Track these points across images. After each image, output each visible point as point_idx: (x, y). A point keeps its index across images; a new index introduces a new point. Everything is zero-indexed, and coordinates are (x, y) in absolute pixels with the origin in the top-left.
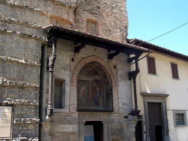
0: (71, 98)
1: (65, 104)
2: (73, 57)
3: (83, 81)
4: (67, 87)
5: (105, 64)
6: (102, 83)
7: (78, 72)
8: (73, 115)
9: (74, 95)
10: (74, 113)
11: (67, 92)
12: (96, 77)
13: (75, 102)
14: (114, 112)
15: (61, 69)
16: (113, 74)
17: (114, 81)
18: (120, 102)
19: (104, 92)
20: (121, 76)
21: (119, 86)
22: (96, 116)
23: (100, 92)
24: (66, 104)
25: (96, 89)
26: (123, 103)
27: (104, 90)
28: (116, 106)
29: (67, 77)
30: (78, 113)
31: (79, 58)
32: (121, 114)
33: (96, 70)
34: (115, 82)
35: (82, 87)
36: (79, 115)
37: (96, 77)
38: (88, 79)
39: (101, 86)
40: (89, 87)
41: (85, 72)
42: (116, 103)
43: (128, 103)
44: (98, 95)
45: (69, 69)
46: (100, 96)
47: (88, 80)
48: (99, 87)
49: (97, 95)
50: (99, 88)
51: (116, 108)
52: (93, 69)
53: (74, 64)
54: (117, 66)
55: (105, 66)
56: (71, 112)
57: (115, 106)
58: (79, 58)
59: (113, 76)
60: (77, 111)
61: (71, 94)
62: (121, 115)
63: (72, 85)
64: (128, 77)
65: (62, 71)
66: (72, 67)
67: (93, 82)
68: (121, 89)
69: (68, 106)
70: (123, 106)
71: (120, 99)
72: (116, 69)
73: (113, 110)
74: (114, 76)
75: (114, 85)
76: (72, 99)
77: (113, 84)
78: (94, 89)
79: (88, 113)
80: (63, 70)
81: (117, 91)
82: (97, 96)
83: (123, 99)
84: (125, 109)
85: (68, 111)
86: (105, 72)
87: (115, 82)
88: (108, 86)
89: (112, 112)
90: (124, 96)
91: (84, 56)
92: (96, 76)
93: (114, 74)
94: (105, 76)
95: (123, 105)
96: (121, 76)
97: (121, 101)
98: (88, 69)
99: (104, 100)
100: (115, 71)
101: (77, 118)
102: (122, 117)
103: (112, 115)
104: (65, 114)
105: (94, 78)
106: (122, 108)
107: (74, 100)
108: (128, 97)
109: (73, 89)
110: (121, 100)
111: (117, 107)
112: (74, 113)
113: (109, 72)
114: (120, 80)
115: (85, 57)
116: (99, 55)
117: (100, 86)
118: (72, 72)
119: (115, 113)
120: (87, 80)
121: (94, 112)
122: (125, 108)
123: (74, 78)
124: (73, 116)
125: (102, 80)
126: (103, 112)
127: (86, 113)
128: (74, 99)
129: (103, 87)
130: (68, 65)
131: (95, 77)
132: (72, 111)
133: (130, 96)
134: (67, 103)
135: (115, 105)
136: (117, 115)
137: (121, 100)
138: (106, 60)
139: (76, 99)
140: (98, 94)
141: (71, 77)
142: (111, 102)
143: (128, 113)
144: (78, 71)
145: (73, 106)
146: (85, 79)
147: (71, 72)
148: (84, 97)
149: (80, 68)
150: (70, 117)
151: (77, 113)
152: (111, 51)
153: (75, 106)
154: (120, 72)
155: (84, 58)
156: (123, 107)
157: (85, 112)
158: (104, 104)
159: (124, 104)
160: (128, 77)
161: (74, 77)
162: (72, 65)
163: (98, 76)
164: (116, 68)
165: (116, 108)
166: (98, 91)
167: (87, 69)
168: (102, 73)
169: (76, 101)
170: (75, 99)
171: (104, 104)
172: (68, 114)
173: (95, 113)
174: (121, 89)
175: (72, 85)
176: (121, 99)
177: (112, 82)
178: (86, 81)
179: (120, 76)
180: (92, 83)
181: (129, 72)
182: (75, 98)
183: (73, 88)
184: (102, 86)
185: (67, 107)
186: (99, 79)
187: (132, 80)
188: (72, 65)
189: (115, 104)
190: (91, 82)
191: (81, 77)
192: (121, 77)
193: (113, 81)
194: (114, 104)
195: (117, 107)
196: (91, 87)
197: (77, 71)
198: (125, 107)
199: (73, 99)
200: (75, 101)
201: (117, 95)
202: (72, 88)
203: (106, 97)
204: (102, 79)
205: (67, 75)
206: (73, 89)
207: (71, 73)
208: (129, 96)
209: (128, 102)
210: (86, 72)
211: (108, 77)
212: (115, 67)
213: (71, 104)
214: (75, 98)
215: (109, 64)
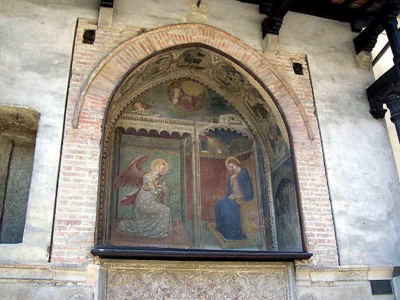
0: (64, 191)
1: (27, 222)
2: (92, 27)
3: (158, 136)
4: (48, 141)
5: (248, 54)
6: (255, 144)
7: (112, 82)
8: (72, 276)
9: (79, 181)
10: (74, 267)
11: (42, 166)
12: (224, 119)
13: (86, 211)
14: (314, 261)
15: (26, 68)
16: (289, 91)
17: (301, 120)
18: (341, 213)
19: (263, 181)
20: (333, 100)
21: (330, 143)
22: (211, 286)
23: (245, 180)
24: (35, 218)
25: (226, 168)
26: (358, 219)
27: (262, 171)
28: (323, 230)
29: (50, 99)
30: (98, 267)
31: (121, 32)
32: (351, 270)
33: (222, 93)
34: (306, 123)
35: (157, 160)
36: (105, 277)
37: (224, 121)
38: (182, 130)
39: (250, 154)
40: (189, 160)
41: (171, 100)
42: (316, 217)
43: (384, 219)
44: (237, 195)
45: (63, 70)
46: (248, 197)
47: (185, 131)
48: (238, 162)
49: (229, 194)
50: (238, 165)
51: (321, 241)
52: (209, 90)
53: (95, 51)
54: (307, 65)
55: (250, 64)
56: (58, 263)
57: (315, 233)
58: (121, 32)
59: (292, 101)
60: (94, 253)
61: (65, 174)
62: (355, 278)
63: (74, 135)
64: (365, 107)
65: (31, 77)
66: (84, 63)
67: (211, 141)
68: (339, 156)
69: (40, 230)
70: (360, 233)
71: (337, 198)
72: (306, 76)
73: (305, 251)
74: (297, 103)
75: (299, 137)
76: (71, 198)
77: (294, 133)
78: (215, 167)
79: (163, 265)
80: (35, 74)
81: (317, 165)
82: (231, 197)
83: (356, 201)
84: (371, 248)
85: (43, 254)
86: (255, 91)
87: (306, 123)
88: (280, 150)
89: (298, 263)
90: (356, 186)
91: (147, 24)
92: (222, 116)
93: (296, 95)
94: (260, 110)
95: (361, 228)
96: (333, 100)
97: (344, 209)
98: (182, 91)
99: (266, 213)
100: (299, 83)
101: (96, 291)
102: (360, 290)
103: (302, 275)
104: (25, 273)
105: (211, 125)
106: (354, 241)
107: (82, 204)
108: (378, 189)
109: (79, 152)
110: (347, 206)
111: (326, 236)
112: (74, 267)
113: (271, 87)
114: (326, 118)
115: (148, 27)
116: (218, 24)
117: (246, 157)
118: (79, 84)
119: (321, 269)
120: (181, 132)
121: (193, 264)
122: (371, 243)
123: (90, 104)
124: (75, 283)
125: (251, 131)
126: (248, 265)
127: (152, 270)
128: (81, 198)
129: (261, 160)
130: (65, 56)
131: (215, 121)
132: (65, 257)
133: (391, 184)
134: (37, 216)
135: (314, 230)
136: (329, 276)
137: (347, 206)
138: (254, 42)
139: (93, 198)
140: (236, 187)
141: (74, 100)
142: (293, 220)
143: (391, 266)
144: (113, 79)
145: (71, 230)
146: (171, 129)
147: (72, 82)
148: (162, 202)
149: (124, 67)
150: (52, 289)
151: (94, 268)
152: (384, 108)
153: (82, 232)
154: (322, 88)
155: (143, 31)
156: (359, 238)
157: (144, 264)
158: (268, 231)
159: (364, 223)
160: (369, 108)
161: (88, 102)
162: (84, 55)
163: (231, 115)
164: (304, 72)
165: (324, 241)
166: (234, 176)
167: (177, 92)
168: (247, 99)
169: (91, 204)
170: (85, 197)
171: (268, 231)
172: (38, 274)
173: (201, 267)
174: (339, 156)
175: (74, 135)
176: (343, 199)
177: (290, 124)
178: (176, 135)
179: (328, 103)
180: (204, 145)
181: (367, 87)
182: (88, 193)
183: (79, 147)
184: (256, 157)
185: (37, 236)
186: (241, 128)
187: (388, 115)
188: (84, 55)
189: (316, 224)
190: (198, 141)
191: (151, 121)
192: (331, 107)
193: (295, 120)
194: (308, 224)
195: (326, 236)
196: (201, 158)
197: (109, 80)
198: (372, 237)
199: (75, 198)
200: (85, 208)
201: (319, 179)
202: (74, 148)
203: (275, 203)
204: (253, 127)
205: (53, 93)
206: (79, 152)
207: (76, 85)
208: (385, 187)
209: (381, 215)
210: (175, 101)
211: (270, 110)
212: (298, 69)
213: (60, 221)
214: (88, 193)
215: (270, 56)
